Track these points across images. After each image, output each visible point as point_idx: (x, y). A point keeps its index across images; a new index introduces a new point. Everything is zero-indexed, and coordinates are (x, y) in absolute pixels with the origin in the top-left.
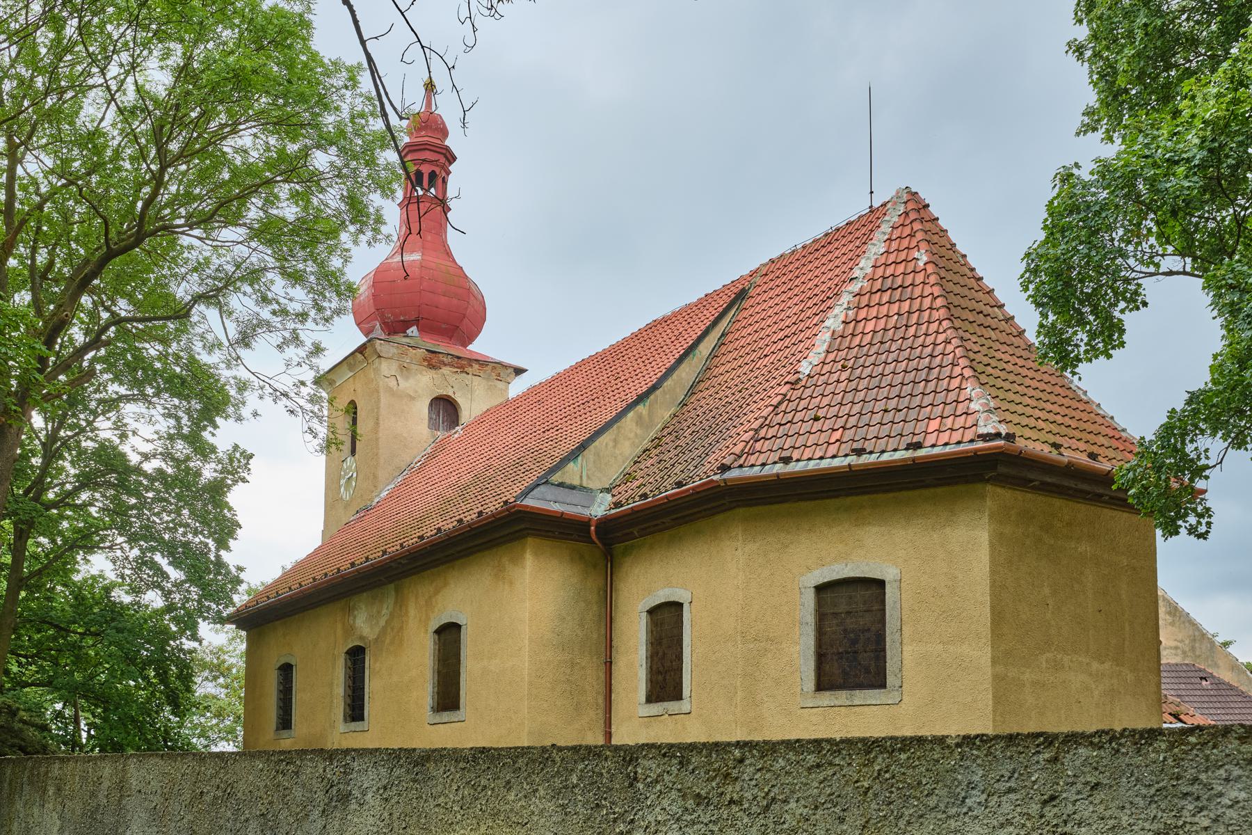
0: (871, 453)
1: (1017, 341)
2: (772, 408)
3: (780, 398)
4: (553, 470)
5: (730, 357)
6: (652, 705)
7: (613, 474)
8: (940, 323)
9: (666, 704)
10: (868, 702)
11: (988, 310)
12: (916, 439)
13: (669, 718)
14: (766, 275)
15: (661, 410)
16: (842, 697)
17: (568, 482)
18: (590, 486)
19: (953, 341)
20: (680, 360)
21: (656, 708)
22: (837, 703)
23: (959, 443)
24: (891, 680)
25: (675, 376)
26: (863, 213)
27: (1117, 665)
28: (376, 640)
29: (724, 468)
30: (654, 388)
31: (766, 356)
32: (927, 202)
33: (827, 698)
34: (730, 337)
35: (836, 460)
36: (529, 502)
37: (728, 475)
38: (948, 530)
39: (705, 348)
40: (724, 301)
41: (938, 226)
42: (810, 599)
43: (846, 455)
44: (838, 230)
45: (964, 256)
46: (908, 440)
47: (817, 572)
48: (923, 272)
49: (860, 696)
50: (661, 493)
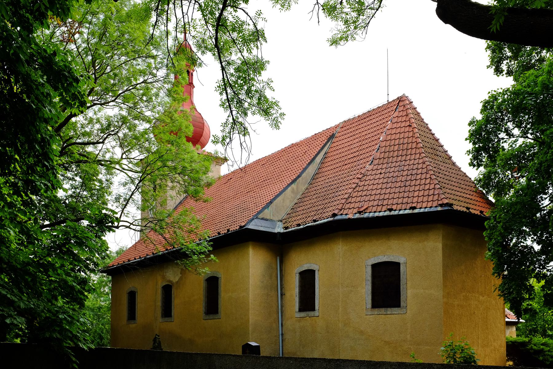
0: (395, 210)
1: (447, 161)
2: (352, 189)
3: (355, 185)
4: (259, 213)
5: (329, 164)
6: (301, 313)
7: (282, 215)
8: (420, 155)
9: (308, 312)
10: (393, 313)
11: (437, 148)
12: (414, 205)
13: (309, 318)
14: (343, 127)
15: (302, 185)
16: (383, 310)
17: (265, 217)
18: (274, 219)
19: (426, 163)
20: (309, 164)
21: (303, 314)
22: (381, 313)
23: (431, 207)
24: (402, 304)
25: (307, 171)
26: (385, 103)
27: (489, 297)
28: (177, 282)
29: (334, 215)
30: (299, 177)
31: (346, 165)
32: (412, 101)
33: (376, 311)
34: (329, 155)
35: (381, 213)
36: (251, 226)
37: (336, 218)
38: (425, 243)
39: (318, 159)
40: (325, 139)
41: (416, 111)
42: (369, 270)
43: (385, 211)
44: (374, 110)
45: (427, 124)
46: (410, 205)
47: (372, 259)
48: (412, 132)
49: (389, 311)
50: (306, 224)
